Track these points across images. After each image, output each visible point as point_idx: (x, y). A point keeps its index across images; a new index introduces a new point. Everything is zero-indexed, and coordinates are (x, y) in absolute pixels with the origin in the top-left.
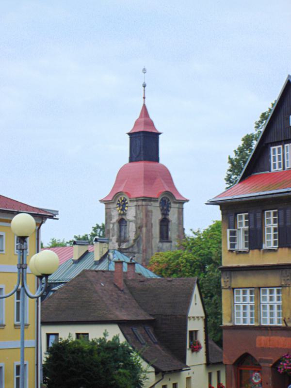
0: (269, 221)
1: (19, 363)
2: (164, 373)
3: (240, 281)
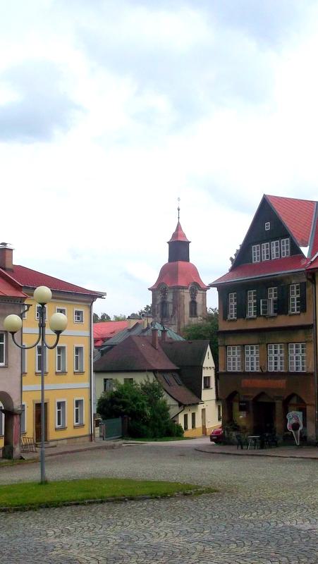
0: (293, 293)
1: (38, 399)
2: (185, 406)
3: (231, 340)
